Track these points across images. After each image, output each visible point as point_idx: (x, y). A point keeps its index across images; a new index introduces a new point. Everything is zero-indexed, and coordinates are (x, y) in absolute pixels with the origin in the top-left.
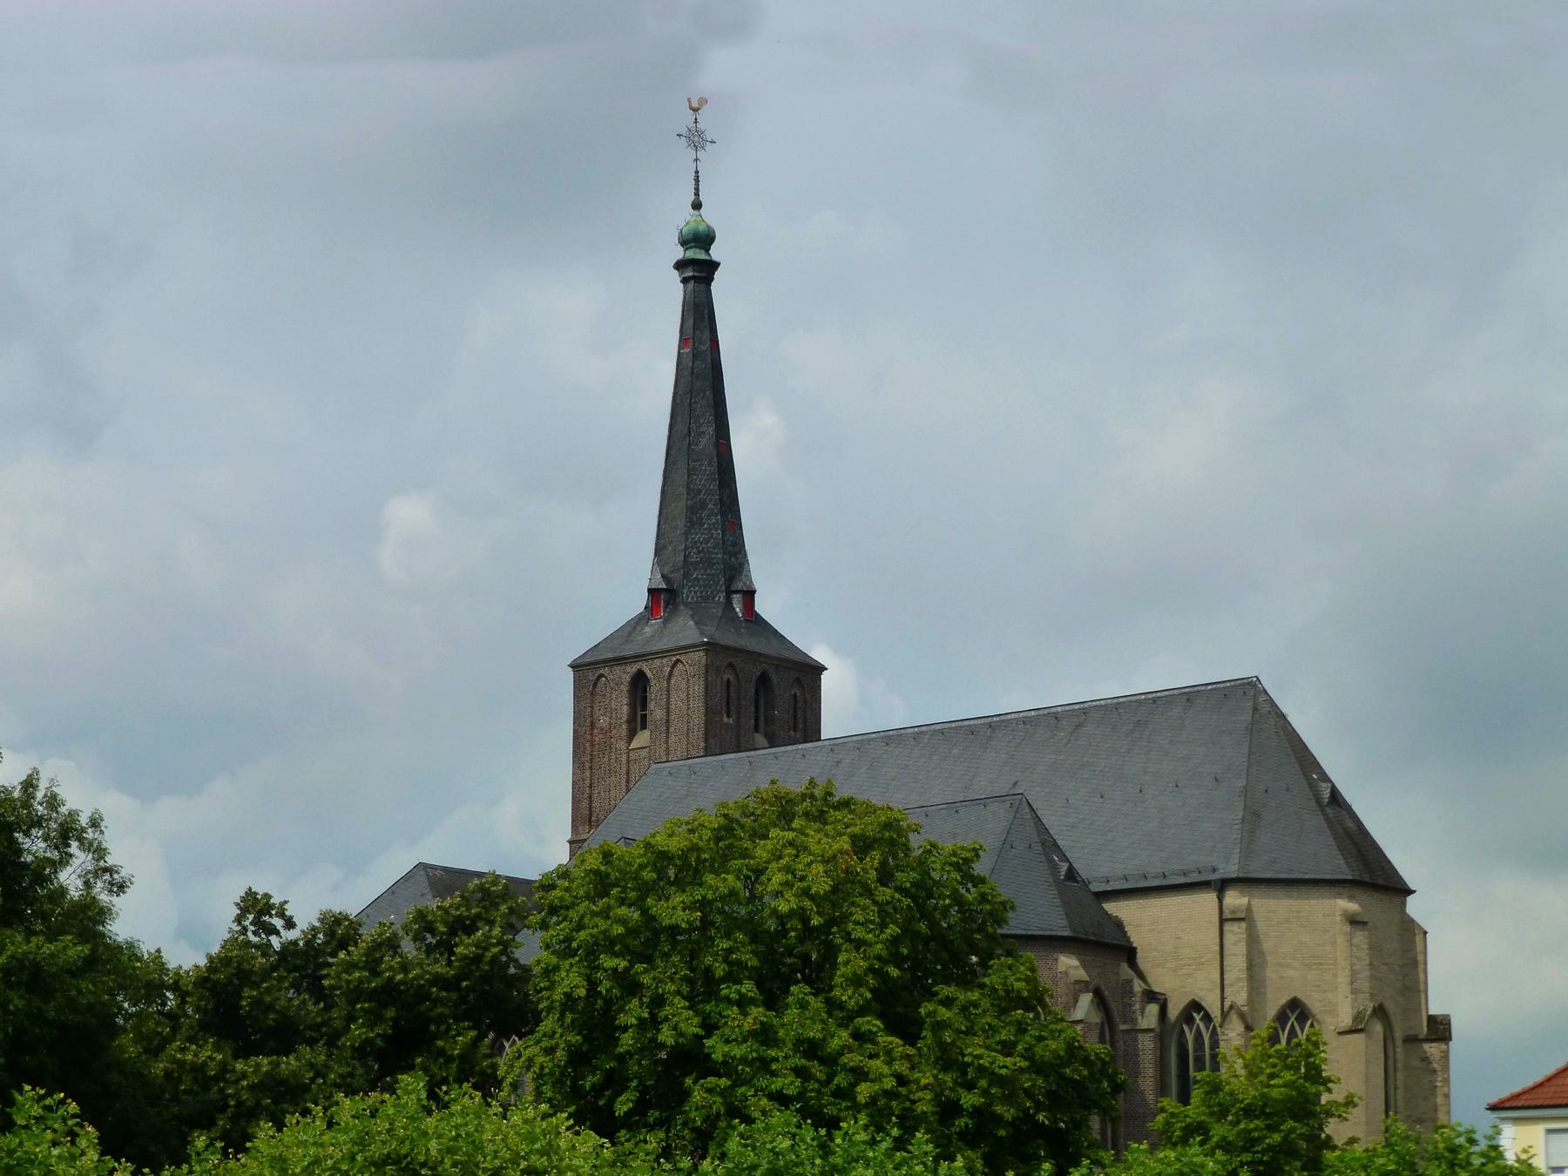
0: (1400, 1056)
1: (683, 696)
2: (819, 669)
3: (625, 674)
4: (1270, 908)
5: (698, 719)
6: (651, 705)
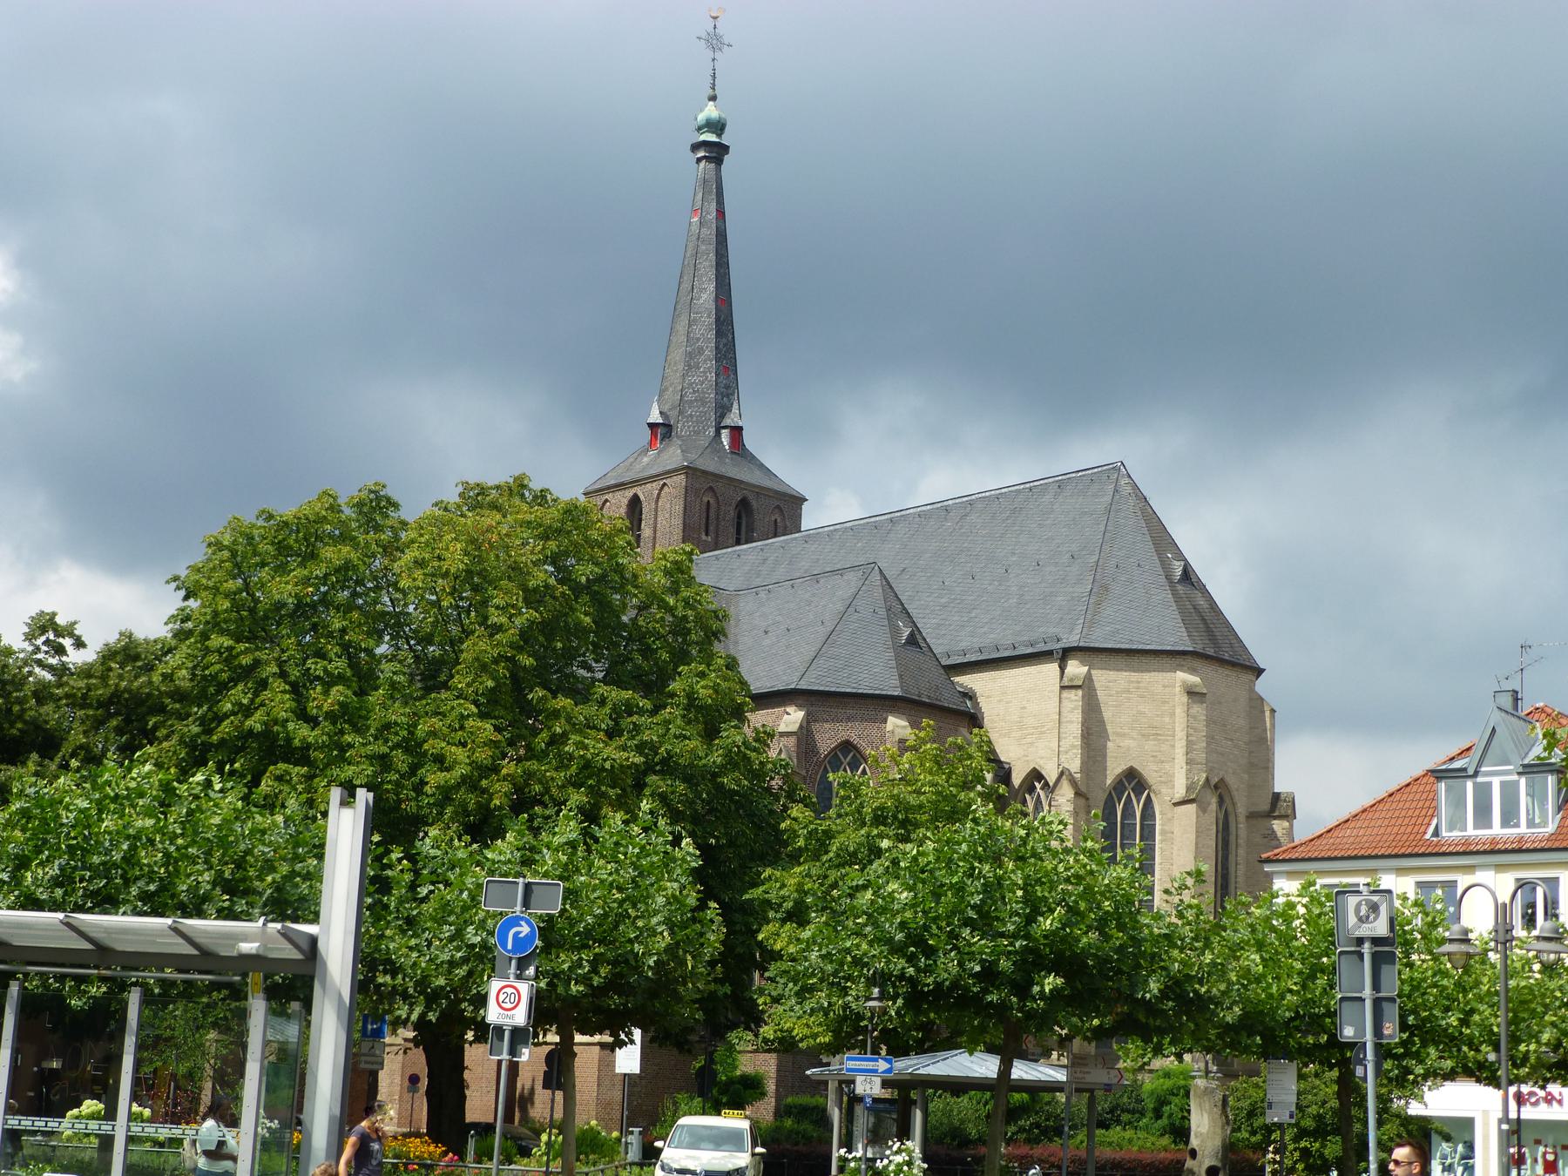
0: (1243, 833)
2: (800, 500)
4: (1111, 682)
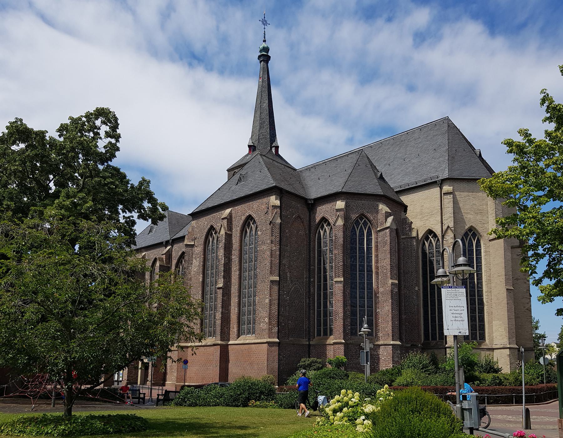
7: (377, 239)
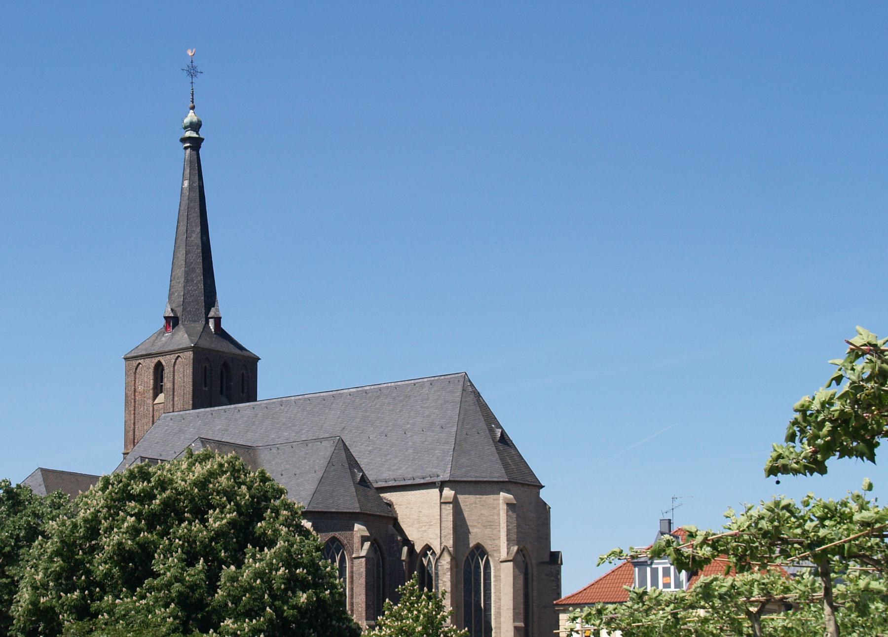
1: (181, 374)
3: (151, 363)
5: (189, 388)
6: (165, 380)
7: (352, 567)
